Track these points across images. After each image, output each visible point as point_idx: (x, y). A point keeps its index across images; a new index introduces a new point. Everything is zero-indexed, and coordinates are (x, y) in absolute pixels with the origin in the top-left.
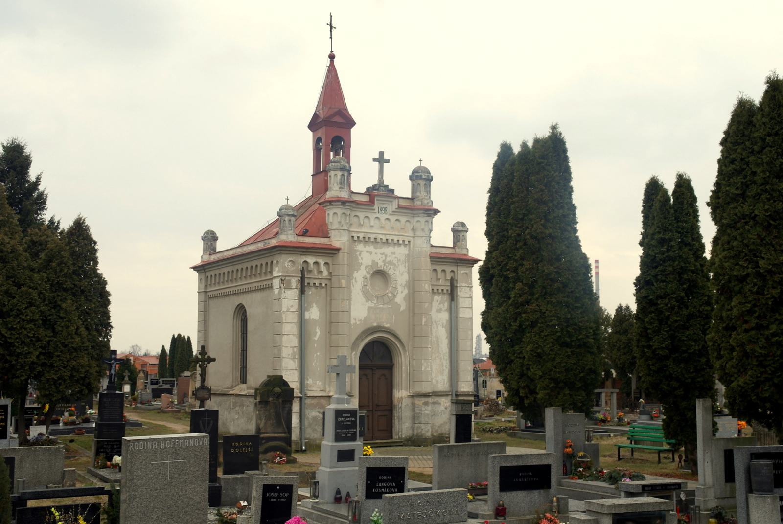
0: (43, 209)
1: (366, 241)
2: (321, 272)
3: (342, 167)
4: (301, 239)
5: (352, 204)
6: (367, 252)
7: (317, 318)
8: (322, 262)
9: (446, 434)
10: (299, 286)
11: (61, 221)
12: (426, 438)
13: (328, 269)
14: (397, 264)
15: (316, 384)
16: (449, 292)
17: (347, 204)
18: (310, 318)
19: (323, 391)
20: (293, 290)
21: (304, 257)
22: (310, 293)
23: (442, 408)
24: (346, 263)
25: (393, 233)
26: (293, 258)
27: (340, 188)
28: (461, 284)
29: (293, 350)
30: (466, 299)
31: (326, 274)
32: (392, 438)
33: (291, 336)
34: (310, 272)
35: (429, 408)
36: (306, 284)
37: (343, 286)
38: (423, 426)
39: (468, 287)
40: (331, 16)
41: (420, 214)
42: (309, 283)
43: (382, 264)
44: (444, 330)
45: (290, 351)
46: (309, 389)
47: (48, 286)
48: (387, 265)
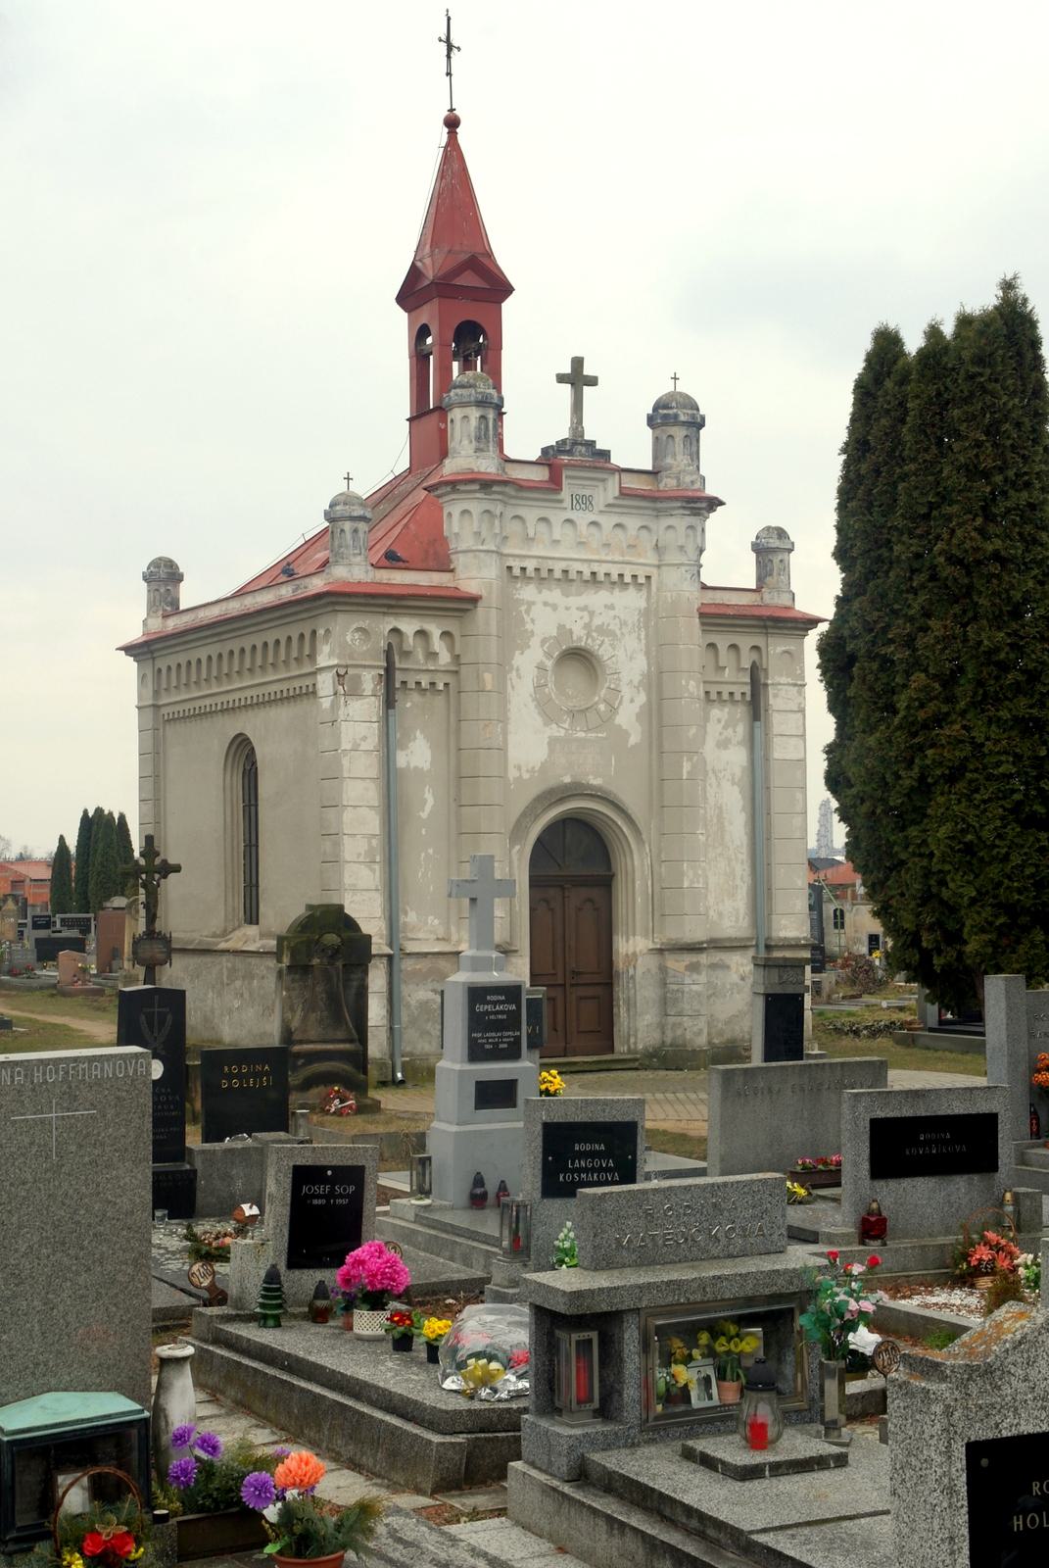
1: (543, 577)
2: (432, 655)
6: (546, 604)
7: (426, 766)
8: (435, 630)
13: (451, 648)
14: (618, 632)
16: (748, 698)
19: (443, 939)
22: (408, 705)
23: (734, 977)
24: (494, 631)
25: (609, 558)
26: (365, 622)
27: (477, 450)
28: (778, 679)
29: (370, 843)
32: (611, 1049)
35: (703, 978)
36: (398, 685)
37: (489, 687)
38: (687, 1022)
39: (795, 685)
41: (674, 508)
42: (404, 683)
43: (583, 633)
44: (736, 789)
46: (410, 935)
48: (594, 634)
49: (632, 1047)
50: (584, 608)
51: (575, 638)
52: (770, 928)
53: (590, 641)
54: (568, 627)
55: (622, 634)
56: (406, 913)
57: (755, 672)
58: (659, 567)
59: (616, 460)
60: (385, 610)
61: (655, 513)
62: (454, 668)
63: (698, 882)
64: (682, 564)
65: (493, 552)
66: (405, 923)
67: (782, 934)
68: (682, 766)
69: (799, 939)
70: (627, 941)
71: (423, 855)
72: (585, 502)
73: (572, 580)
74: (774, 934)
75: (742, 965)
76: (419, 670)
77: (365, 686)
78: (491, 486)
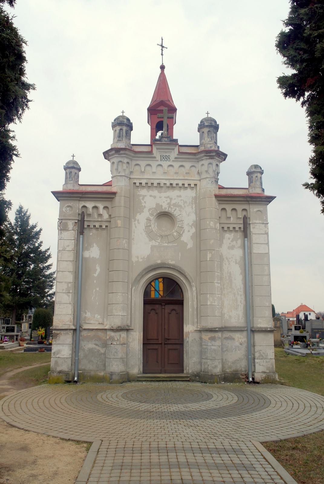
1: (150, 186)
2: (100, 215)
3: (119, 122)
5: (127, 152)
6: (151, 196)
7: (97, 257)
8: (101, 206)
9: (241, 371)
12: (212, 375)
14: (183, 206)
15: (94, 317)
16: (242, 229)
17: (121, 152)
18: (90, 257)
19: (102, 324)
20: (70, 232)
21: (83, 202)
22: (91, 234)
23: (237, 344)
24: (123, 204)
25: (178, 178)
27: (118, 140)
28: (255, 221)
29: (68, 285)
30: (261, 236)
31: (106, 216)
32: (182, 371)
33: (67, 273)
34: (89, 215)
35: (218, 343)
36: (86, 226)
37: (119, 225)
38: (209, 362)
39: (263, 223)
40: (162, 39)
41: (202, 157)
42: (89, 226)
43: (167, 206)
44: (237, 266)
45: (65, 286)
46: (87, 322)
48: (172, 206)
49: (187, 371)
50: (168, 197)
51: (163, 208)
52: (253, 323)
53: (170, 209)
54: (160, 204)
55: (185, 206)
56: (86, 313)
57: (245, 219)
58: (200, 180)
59: (180, 143)
60: (79, 199)
61: (197, 160)
62: (109, 220)
63: (215, 303)
64: (207, 178)
65: (123, 176)
66: (85, 317)
67: (259, 326)
68: (207, 256)
69: (267, 328)
70: (186, 327)
71: (94, 290)
72: (167, 158)
73: (162, 187)
74: (255, 326)
75: (240, 338)
76: (95, 221)
77: (69, 226)
78: (120, 151)
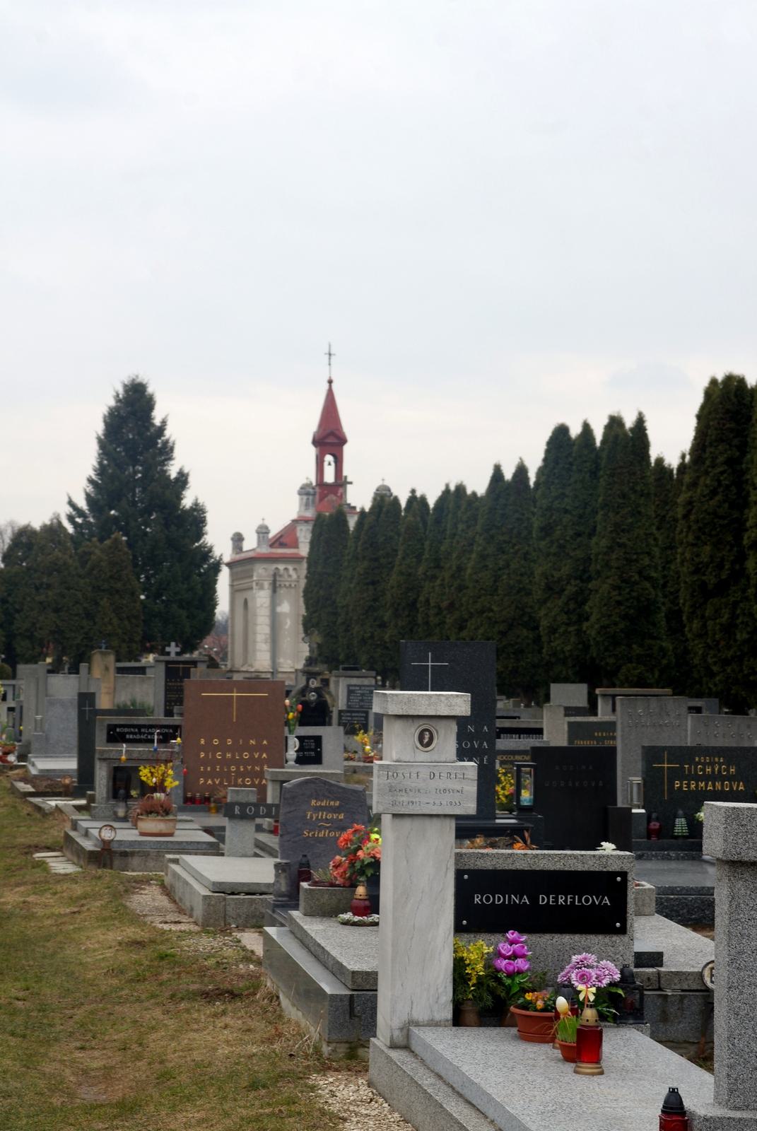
0: (170, 459)
2: (290, 576)
4: (274, 550)
8: (290, 568)
10: (271, 587)
11: (333, 378)
13: (297, 573)
26: (265, 566)
34: (280, 576)
47: (90, 589)
